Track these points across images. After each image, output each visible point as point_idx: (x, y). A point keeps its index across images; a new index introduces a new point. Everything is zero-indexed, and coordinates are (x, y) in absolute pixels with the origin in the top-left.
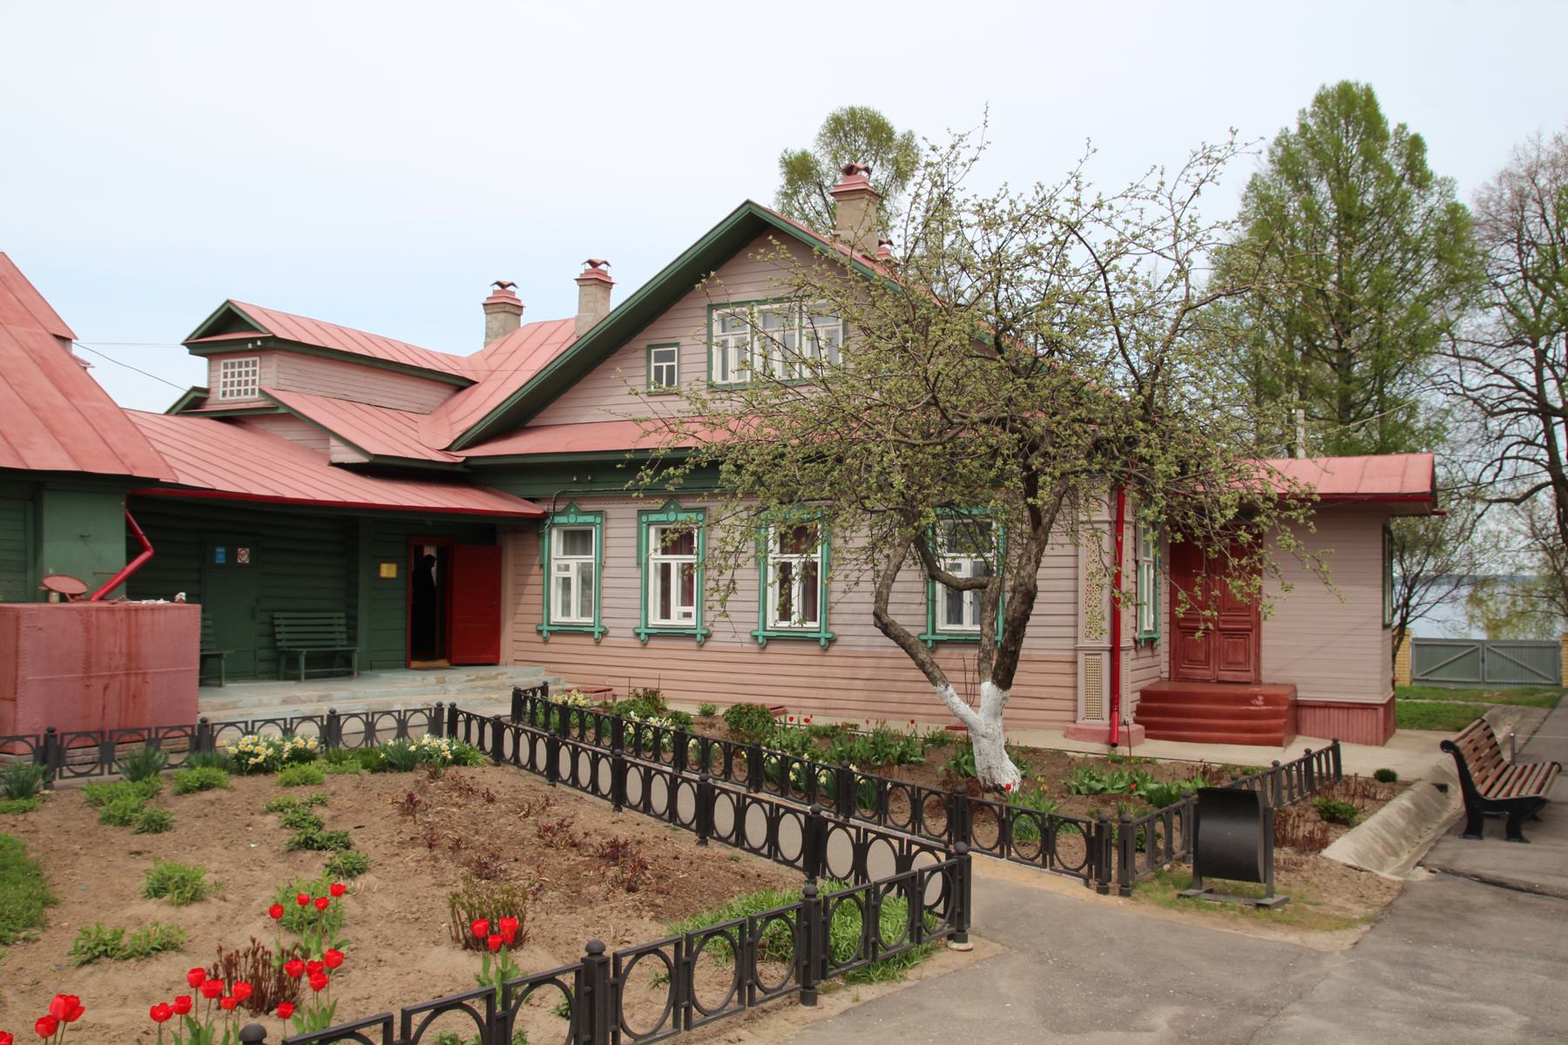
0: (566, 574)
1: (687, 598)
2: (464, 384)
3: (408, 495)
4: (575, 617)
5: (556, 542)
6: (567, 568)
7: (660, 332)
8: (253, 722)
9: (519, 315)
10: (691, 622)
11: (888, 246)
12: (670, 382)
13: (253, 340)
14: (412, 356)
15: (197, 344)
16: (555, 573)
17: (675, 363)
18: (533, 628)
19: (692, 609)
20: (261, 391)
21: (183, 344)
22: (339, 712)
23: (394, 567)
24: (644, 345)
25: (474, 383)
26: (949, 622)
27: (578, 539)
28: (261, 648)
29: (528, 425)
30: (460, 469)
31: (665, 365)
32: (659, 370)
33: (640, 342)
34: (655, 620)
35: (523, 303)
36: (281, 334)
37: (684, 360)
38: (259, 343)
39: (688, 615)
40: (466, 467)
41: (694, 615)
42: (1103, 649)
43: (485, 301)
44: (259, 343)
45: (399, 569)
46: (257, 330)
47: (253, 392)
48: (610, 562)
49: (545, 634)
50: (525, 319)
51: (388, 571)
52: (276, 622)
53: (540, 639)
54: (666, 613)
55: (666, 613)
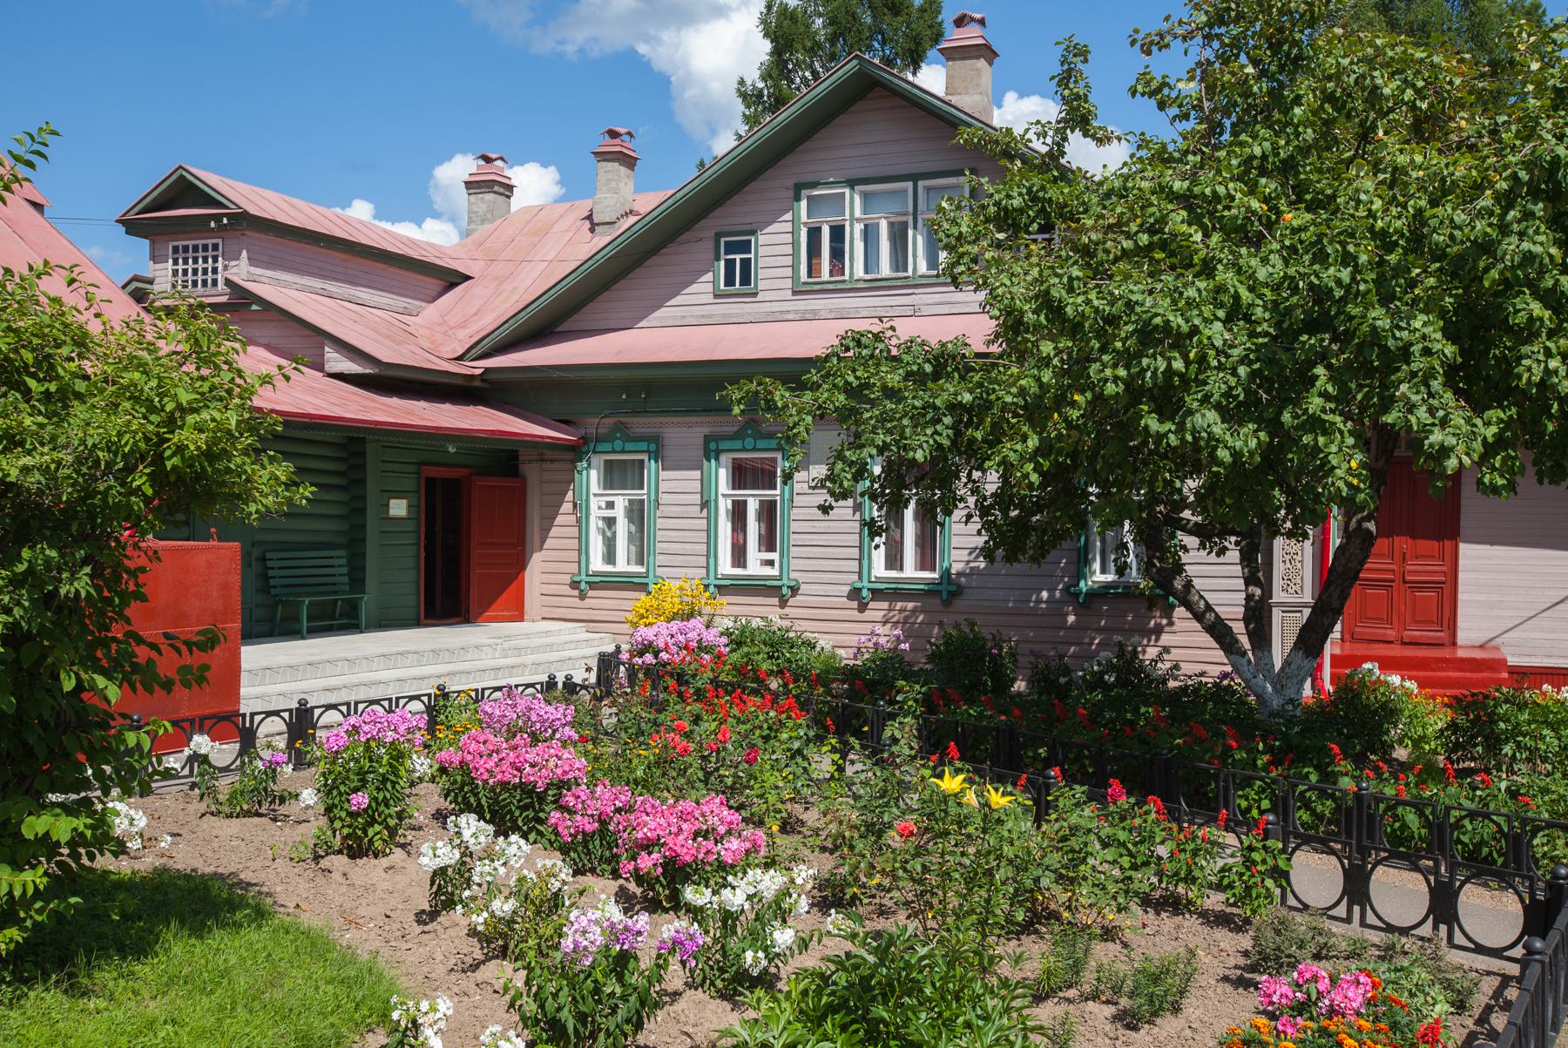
0: (609, 513)
1: (768, 542)
2: (455, 280)
3: (410, 413)
4: (622, 565)
5: (592, 478)
6: (610, 505)
7: (730, 216)
8: (356, 703)
9: (509, 197)
10: (775, 572)
11: (499, 163)
12: (746, 280)
13: (217, 218)
14: (401, 246)
15: (133, 226)
16: (595, 512)
17: (752, 256)
18: (567, 579)
19: (775, 556)
20: (228, 282)
21: (117, 221)
22: (452, 687)
23: (404, 503)
24: (712, 234)
25: (468, 278)
26: (733, 566)
27: (618, 476)
28: (257, 606)
29: (558, 329)
30: (477, 383)
31: (738, 257)
32: (730, 265)
33: (708, 227)
34: (726, 567)
35: (513, 182)
36: (253, 211)
37: (762, 251)
38: (225, 221)
39: (771, 563)
40: (483, 380)
41: (777, 565)
42: (1305, 605)
43: (467, 178)
44: (225, 221)
45: (409, 506)
46: (220, 205)
47: (215, 282)
48: (664, 498)
49: (583, 586)
50: (517, 202)
51: (399, 508)
52: (271, 573)
53: (576, 593)
54: (739, 557)
55: (739, 557)
